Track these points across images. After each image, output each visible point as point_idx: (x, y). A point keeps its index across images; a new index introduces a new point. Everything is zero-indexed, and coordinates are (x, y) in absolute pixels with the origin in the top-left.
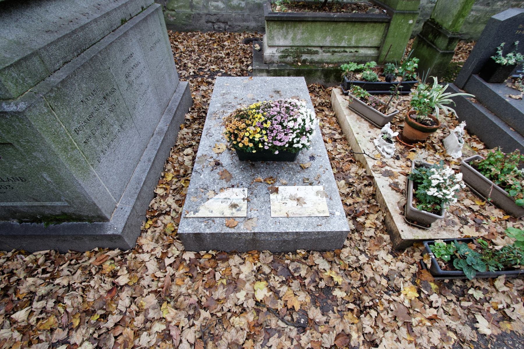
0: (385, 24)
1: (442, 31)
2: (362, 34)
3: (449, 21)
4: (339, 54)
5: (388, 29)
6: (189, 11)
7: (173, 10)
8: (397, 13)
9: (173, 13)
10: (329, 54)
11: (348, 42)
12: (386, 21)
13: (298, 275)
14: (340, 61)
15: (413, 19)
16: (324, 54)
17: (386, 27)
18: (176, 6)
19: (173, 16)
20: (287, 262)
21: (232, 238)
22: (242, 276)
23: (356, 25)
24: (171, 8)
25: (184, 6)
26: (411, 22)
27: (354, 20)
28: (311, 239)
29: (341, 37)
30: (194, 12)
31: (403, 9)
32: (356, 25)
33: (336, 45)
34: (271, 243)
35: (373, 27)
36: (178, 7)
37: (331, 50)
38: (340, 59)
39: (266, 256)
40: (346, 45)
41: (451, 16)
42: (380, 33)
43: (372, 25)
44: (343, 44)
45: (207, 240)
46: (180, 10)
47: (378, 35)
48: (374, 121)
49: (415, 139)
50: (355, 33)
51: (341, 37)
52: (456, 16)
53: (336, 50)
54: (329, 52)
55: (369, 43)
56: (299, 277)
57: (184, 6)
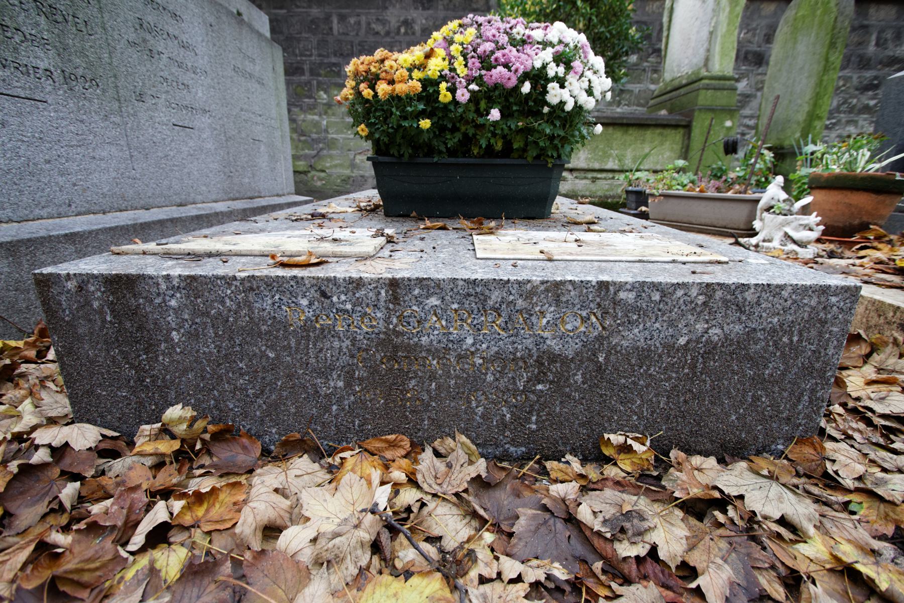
0: (682, 131)
1: (785, 151)
2: (643, 148)
3: (793, 133)
4: (605, 182)
5: (689, 138)
6: (347, 172)
7: (323, 171)
8: (700, 110)
9: (323, 175)
10: (588, 182)
11: (619, 161)
12: (683, 123)
13: (641, 550)
14: (607, 193)
15: (731, 119)
16: (577, 181)
17: (684, 135)
18: (328, 165)
19: (321, 180)
20: (558, 489)
21: (286, 326)
22: (294, 539)
23: (631, 131)
24: (319, 167)
25: (341, 166)
26: (728, 124)
27: (625, 121)
28: (670, 348)
29: (605, 153)
30: (356, 173)
31: (708, 103)
32: (630, 132)
33: (597, 166)
34: (473, 382)
35: (661, 134)
36: (331, 167)
37: (590, 175)
38: (607, 190)
39: (449, 466)
40: (616, 167)
41: (795, 126)
42: (674, 146)
43: (658, 131)
44: (610, 165)
45: (168, 339)
46: (334, 170)
47: (672, 150)
48: (724, 224)
49: (856, 222)
50: (630, 145)
51: (605, 153)
52: (805, 120)
53: (599, 176)
54: (586, 178)
55: (657, 163)
56: (650, 567)
57: (341, 166)
